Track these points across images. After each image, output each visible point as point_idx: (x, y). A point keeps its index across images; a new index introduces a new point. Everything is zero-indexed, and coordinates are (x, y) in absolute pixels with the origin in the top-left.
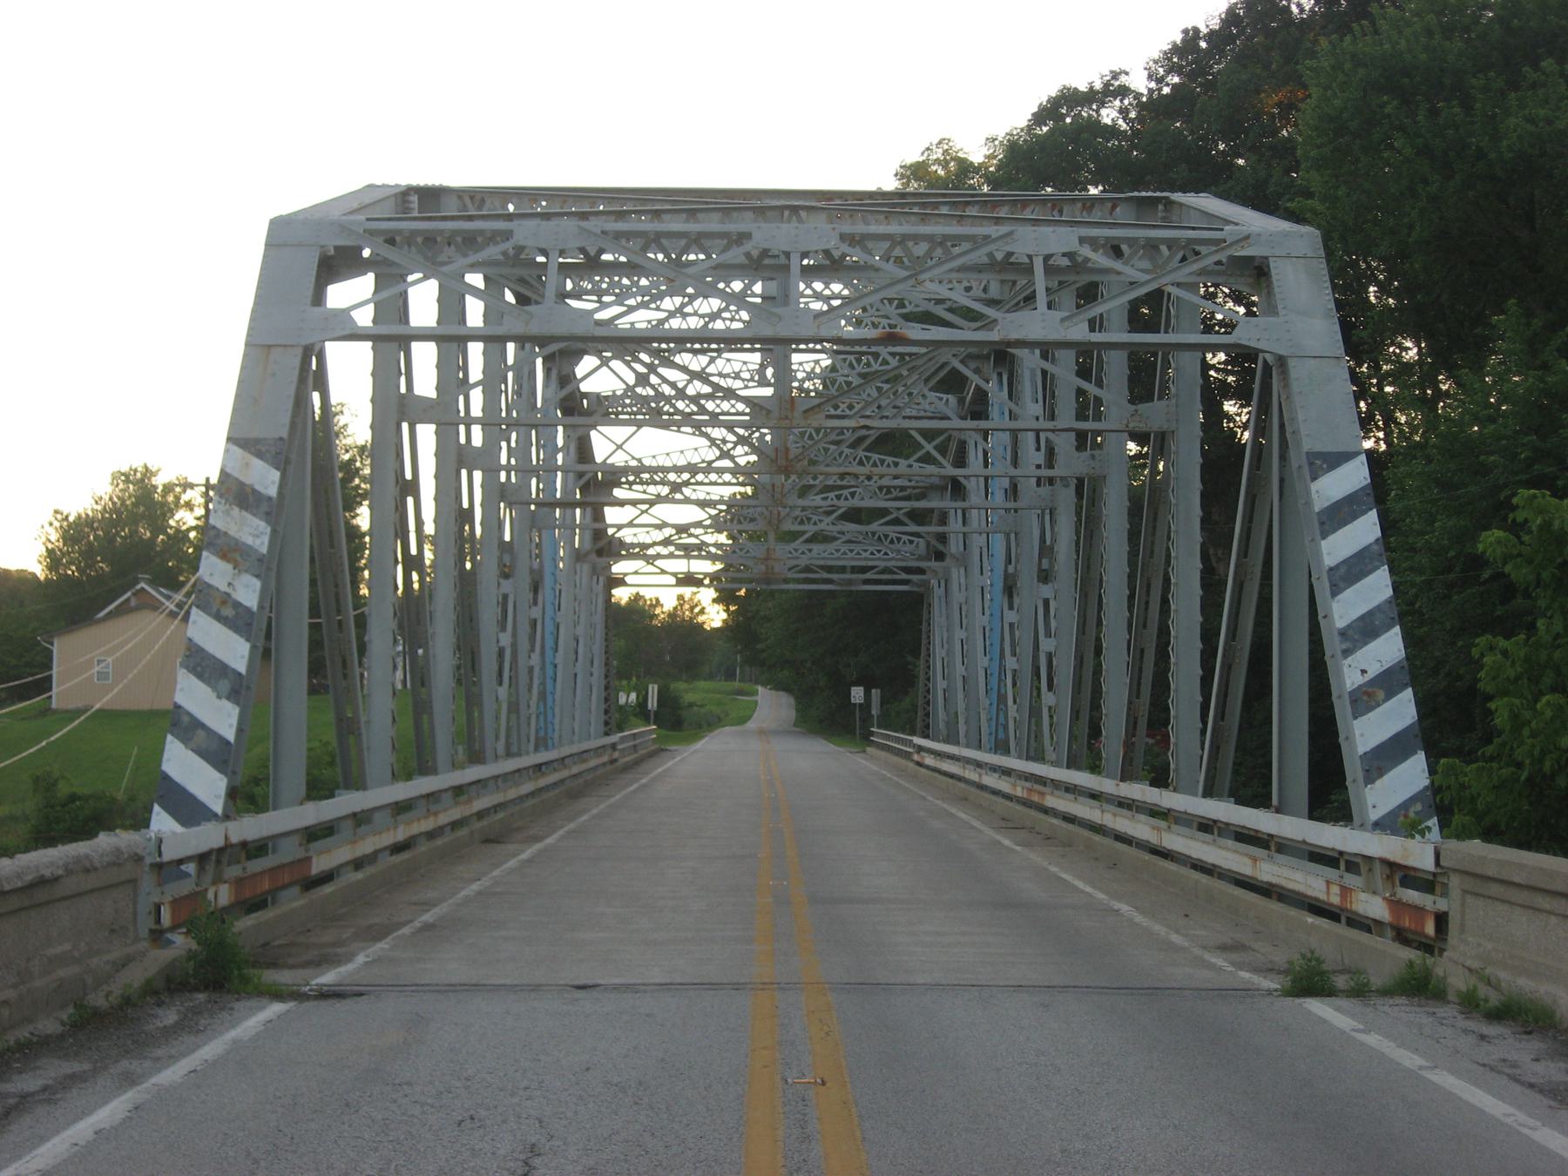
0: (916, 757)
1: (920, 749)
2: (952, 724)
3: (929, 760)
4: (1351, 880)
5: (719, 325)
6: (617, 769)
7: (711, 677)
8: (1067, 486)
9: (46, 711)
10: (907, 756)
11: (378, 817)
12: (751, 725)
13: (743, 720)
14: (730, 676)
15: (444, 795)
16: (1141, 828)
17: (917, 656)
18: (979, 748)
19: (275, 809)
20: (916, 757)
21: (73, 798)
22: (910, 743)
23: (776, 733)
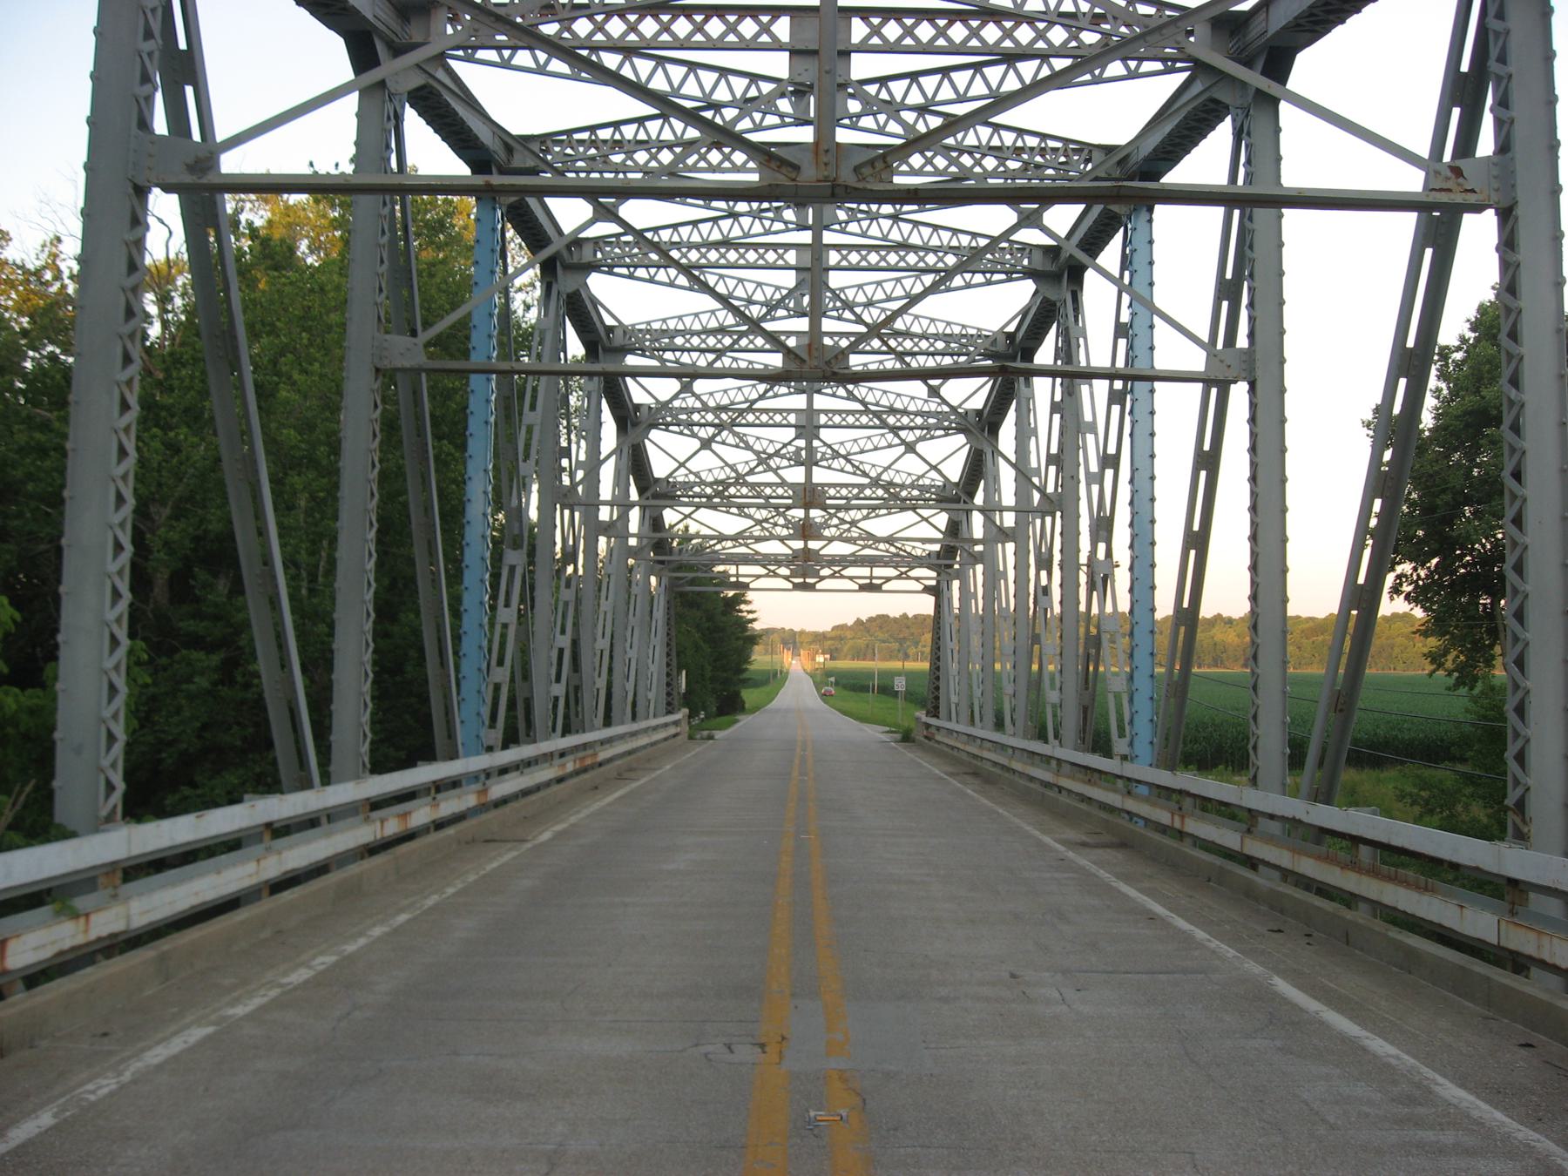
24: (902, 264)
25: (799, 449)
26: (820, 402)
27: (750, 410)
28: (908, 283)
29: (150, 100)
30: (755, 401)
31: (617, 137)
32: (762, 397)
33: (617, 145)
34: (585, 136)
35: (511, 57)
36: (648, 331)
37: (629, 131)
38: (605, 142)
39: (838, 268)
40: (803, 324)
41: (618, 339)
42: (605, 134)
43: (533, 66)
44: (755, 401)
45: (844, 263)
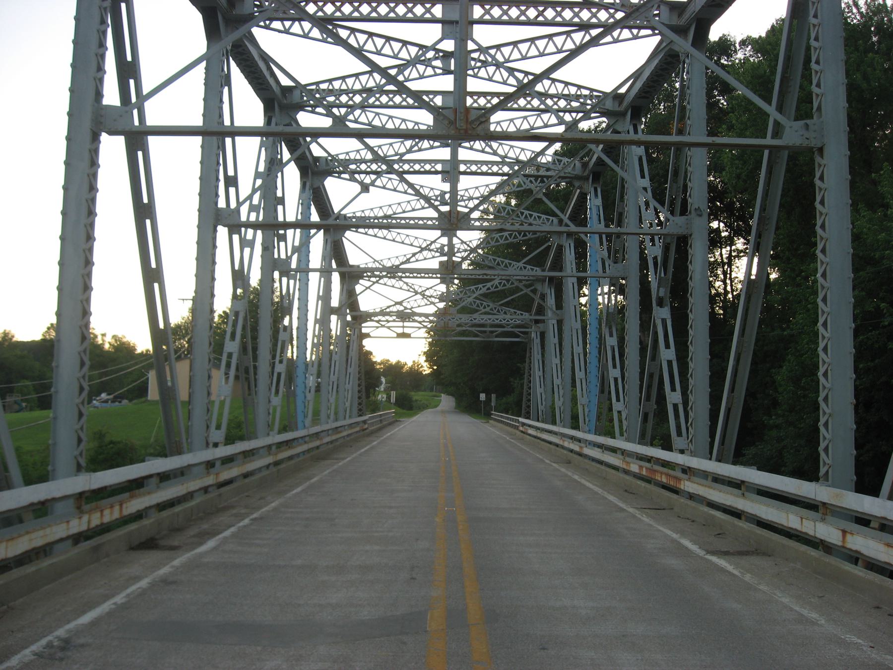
0: (521, 428)
1: (524, 424)
2: (528, 413)
3: (531, 431)
4: (582, 445)
5: (408, 143)
6: (365, 434)
7: (425, 390)
8: (700, 216)
9: (147, 401)
10: (516, 428)
11: (59, 508)
12: (439, 408)
13: (436, 406)
14: (432, 390)
15: (261, 450)
16: (790, 518)
17: (522, 378)
18: (538, 421)
19: (53, 480)
20: (521, 428)
21: (112, 442)
22: (519, 422)
23: (449, 412)
24: (529, 106)
25: (443, 246)
26: (463, 154)
27: (401, 161)
28: (531, 120)
29: (104, 33)
30: (404, 154)
31: (331, 87)
32: (409, 151)
33: (331, 92)
34: (314, 87)
35: (270, 24)
36: (354, 217)
37: (337, 85)
38: (324, 90)
39: (465, 173)
40: (447, 83)
41: (322, 166)
42: (324, 86)
43: (282, 29)
44: (404, 154)
45: (487, 17)
